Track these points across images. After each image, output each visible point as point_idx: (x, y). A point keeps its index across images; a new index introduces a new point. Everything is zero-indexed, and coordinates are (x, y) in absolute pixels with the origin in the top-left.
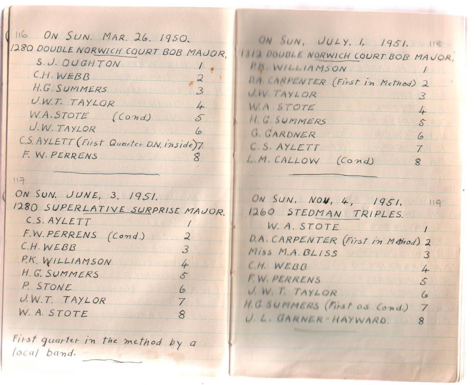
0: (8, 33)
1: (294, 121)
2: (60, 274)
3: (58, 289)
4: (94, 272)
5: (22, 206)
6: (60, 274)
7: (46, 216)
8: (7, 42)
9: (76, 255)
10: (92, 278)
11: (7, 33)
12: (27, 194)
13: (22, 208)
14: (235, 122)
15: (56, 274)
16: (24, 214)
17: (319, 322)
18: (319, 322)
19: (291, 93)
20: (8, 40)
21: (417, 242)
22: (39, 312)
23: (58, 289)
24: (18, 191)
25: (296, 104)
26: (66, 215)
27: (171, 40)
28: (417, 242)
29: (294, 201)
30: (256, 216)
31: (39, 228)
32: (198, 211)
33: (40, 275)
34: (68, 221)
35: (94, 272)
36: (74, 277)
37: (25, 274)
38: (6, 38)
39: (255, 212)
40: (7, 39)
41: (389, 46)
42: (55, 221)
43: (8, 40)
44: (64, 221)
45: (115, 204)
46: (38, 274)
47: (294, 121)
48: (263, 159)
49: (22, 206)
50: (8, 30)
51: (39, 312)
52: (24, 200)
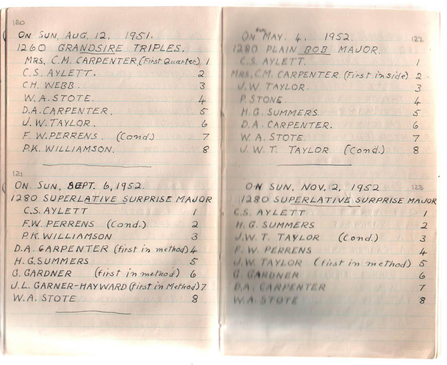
0: (5, 33)
1: (65, 261)
2: (51, 261)
3: (105, 238)
4: (84, 260)
5: (20, 198)
6: (51, 261)
7: (42, 206)
8: (4, 42)
9: (282, 107)
10: (83, 265)
11: (4, 33)
12: (25, 186)
13: (21, 200)
14: (222, 114)
15: (47, 262)
16: (22, 204)
17: (321, 290)
18: (321, 290)
19: (282, 85)
20: (5, 40)
21: (408, 264)
22: (31, 297)
23: (105, 238)
24: (18, 182)
25: (365, 46)
26: (63, 206)
27: (135, 37)
28: (408, 264)
29: (291, 189)
30: (249, 203)
31: (37, 218)
32: (189, 199)
33: (33, 263)
34: (63, 210)
35: (84, 260)
36: (65, 265)
37: (18, 262)
38: (4, 38)
39: (249, 199)
40: (5, 38)
41: (123, 190)
42: (51, 211)
43: (5, 40)
44: (59, 211)
45: (107, 193)
46: (31, 262)
47: (65, 261)
48: (257, 150)
49: (20, 198)
50: (5, 30)
51: (31, 297)
52: (23, 192)
